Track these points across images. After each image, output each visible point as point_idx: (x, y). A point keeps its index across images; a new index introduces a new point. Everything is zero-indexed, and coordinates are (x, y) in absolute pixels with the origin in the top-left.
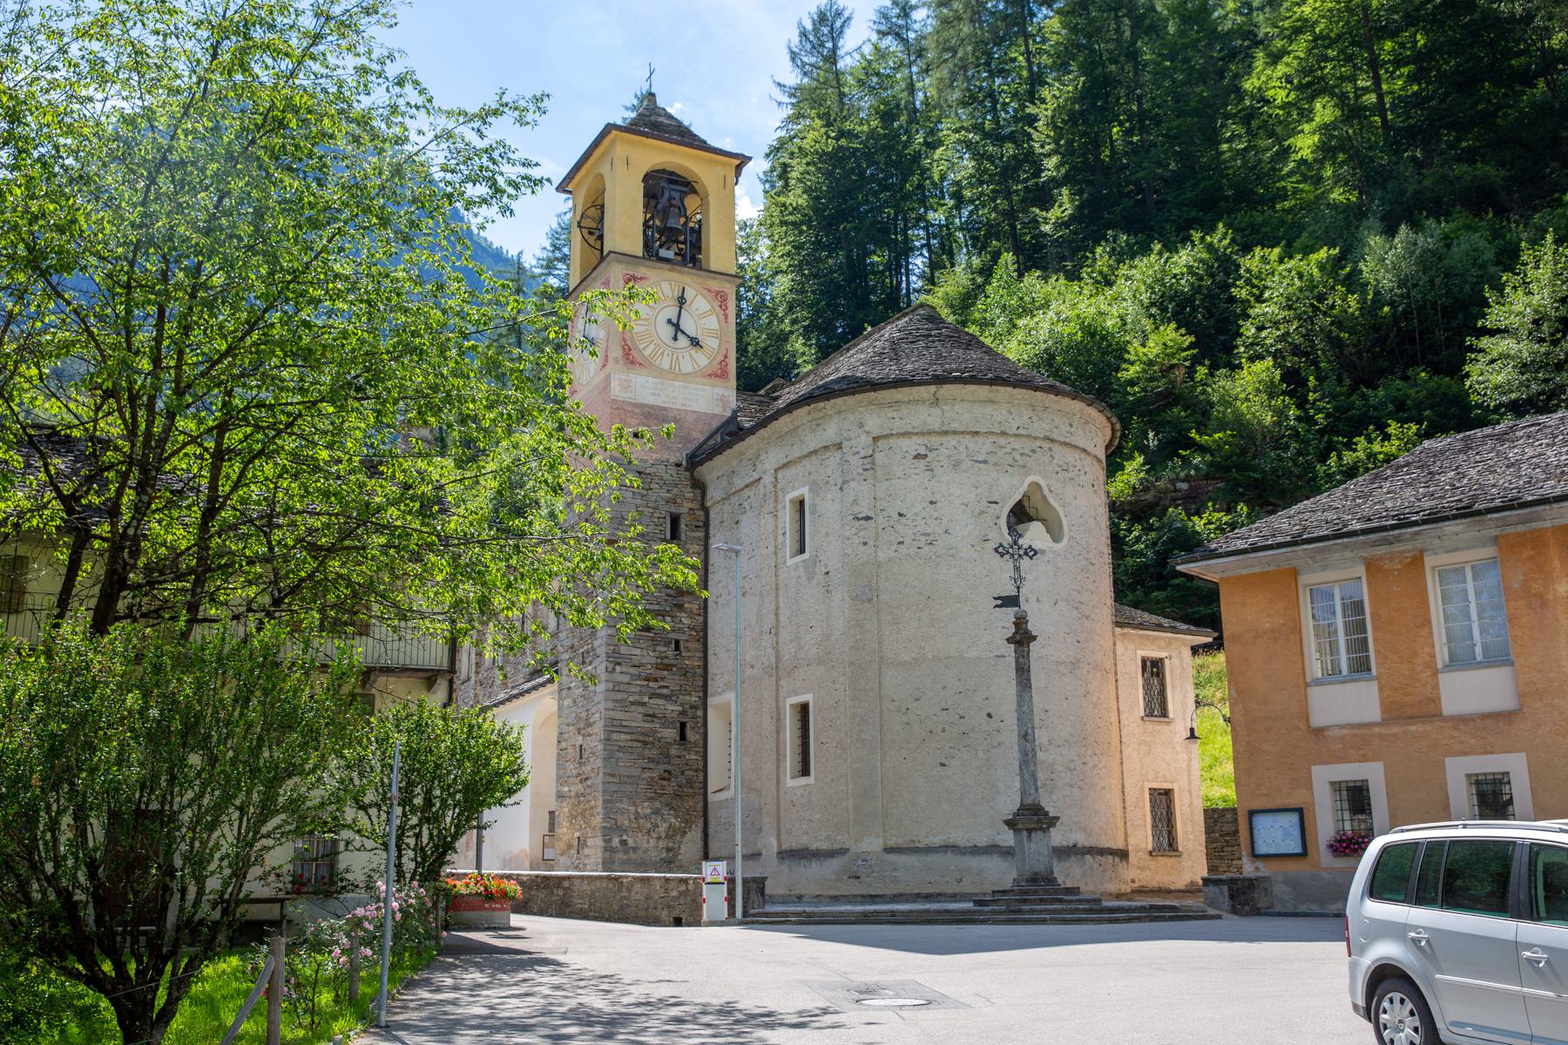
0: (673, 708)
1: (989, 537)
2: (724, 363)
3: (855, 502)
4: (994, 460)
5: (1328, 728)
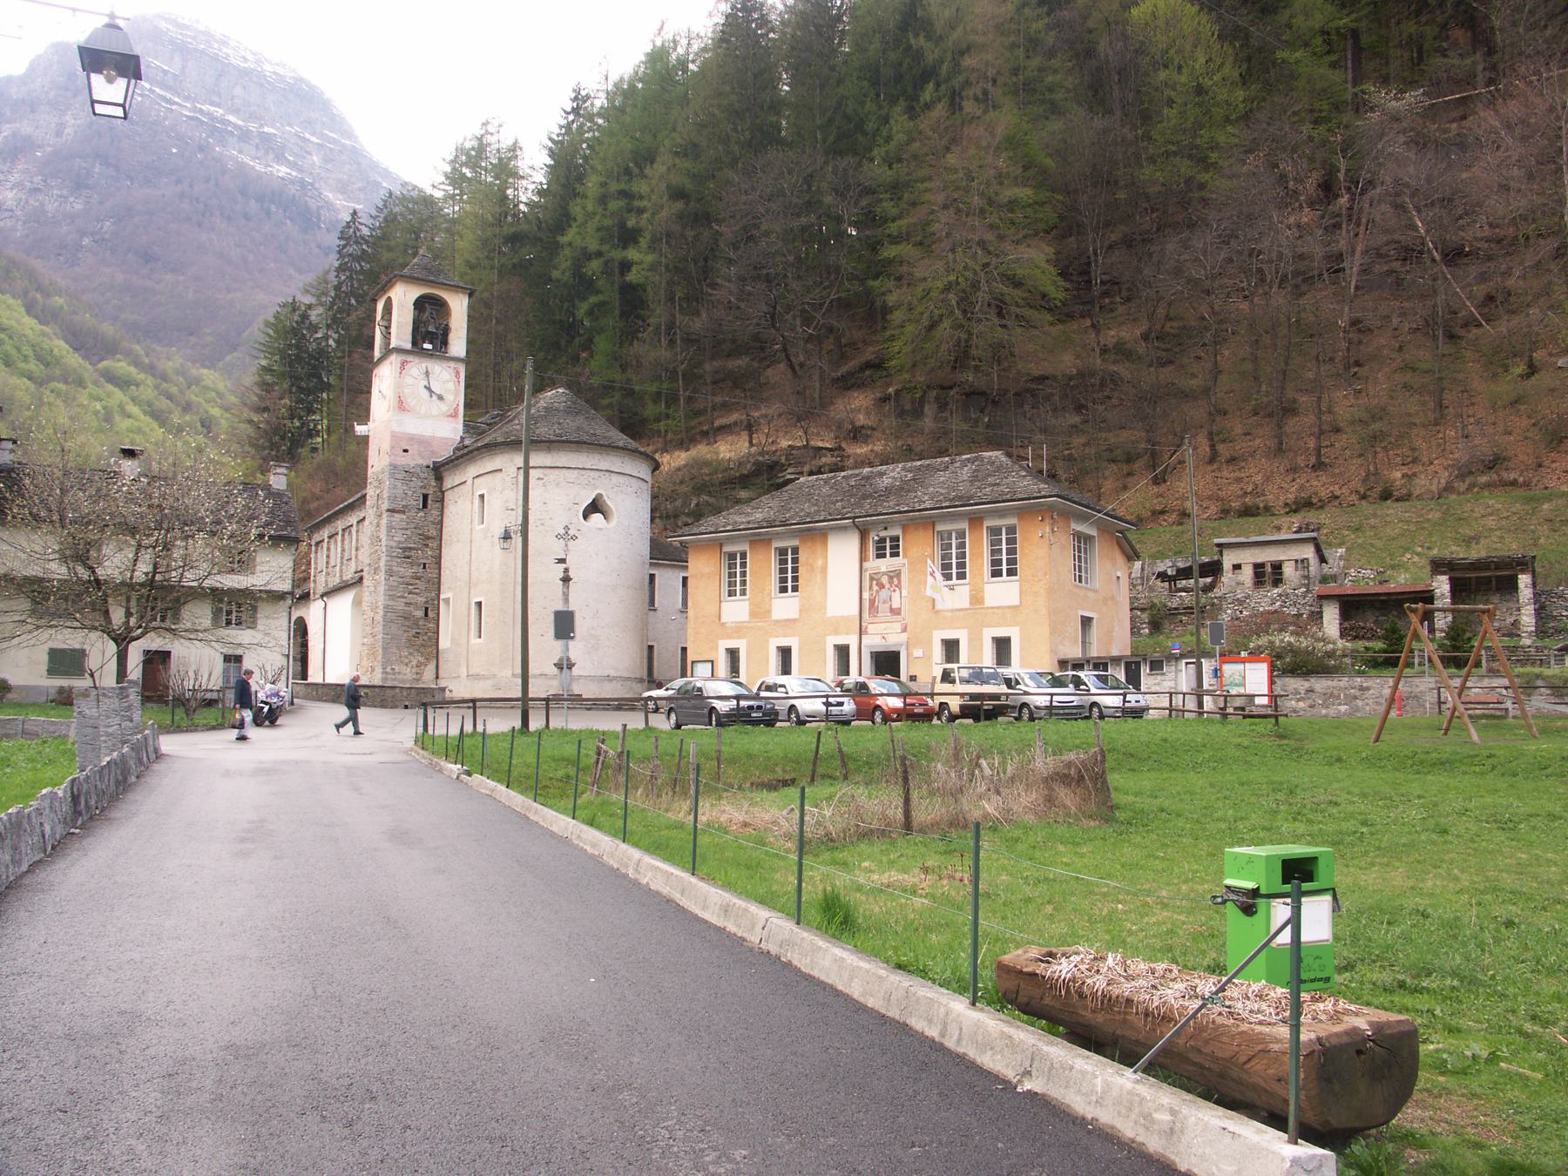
0: (421, 600)
2: (456, 410)
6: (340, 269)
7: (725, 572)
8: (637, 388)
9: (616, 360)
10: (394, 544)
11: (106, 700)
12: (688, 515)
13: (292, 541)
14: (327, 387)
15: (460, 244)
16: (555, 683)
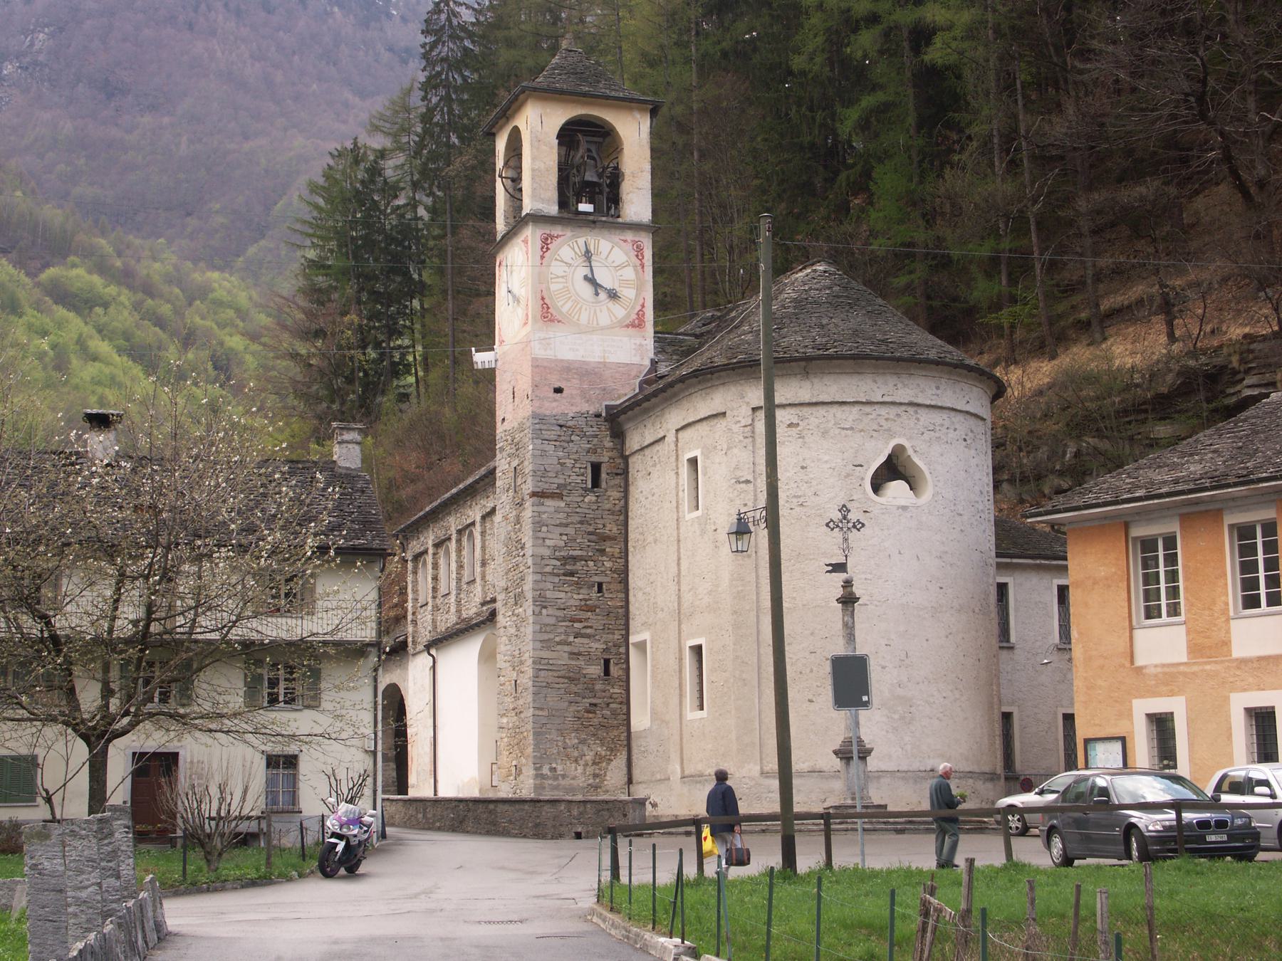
0: (597, 646)
1: (854, 498)
2: (640, 315)
3: (737, 468)
4: (860, 427)
5: (1145, 667)
6: (428, 86)
7: (1137, 573)
8: (955, 253)
9: (914, 204)
10: (547, 552)
11: (77, 843)
12: (1061, 474)
13: (375, 555)
14: (421, 289)
15: (631, 24)
16: (838, 785)
